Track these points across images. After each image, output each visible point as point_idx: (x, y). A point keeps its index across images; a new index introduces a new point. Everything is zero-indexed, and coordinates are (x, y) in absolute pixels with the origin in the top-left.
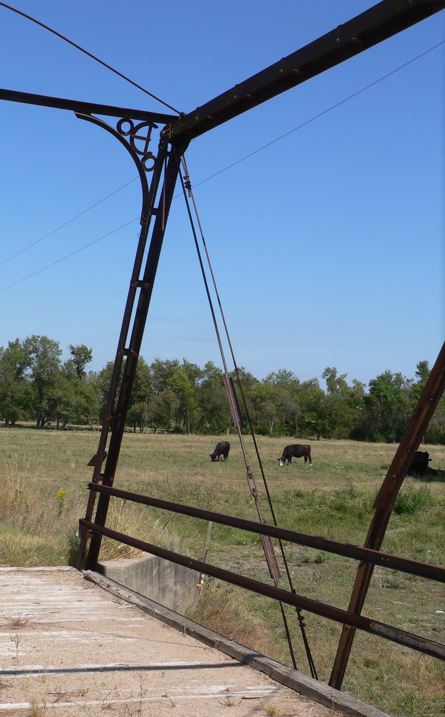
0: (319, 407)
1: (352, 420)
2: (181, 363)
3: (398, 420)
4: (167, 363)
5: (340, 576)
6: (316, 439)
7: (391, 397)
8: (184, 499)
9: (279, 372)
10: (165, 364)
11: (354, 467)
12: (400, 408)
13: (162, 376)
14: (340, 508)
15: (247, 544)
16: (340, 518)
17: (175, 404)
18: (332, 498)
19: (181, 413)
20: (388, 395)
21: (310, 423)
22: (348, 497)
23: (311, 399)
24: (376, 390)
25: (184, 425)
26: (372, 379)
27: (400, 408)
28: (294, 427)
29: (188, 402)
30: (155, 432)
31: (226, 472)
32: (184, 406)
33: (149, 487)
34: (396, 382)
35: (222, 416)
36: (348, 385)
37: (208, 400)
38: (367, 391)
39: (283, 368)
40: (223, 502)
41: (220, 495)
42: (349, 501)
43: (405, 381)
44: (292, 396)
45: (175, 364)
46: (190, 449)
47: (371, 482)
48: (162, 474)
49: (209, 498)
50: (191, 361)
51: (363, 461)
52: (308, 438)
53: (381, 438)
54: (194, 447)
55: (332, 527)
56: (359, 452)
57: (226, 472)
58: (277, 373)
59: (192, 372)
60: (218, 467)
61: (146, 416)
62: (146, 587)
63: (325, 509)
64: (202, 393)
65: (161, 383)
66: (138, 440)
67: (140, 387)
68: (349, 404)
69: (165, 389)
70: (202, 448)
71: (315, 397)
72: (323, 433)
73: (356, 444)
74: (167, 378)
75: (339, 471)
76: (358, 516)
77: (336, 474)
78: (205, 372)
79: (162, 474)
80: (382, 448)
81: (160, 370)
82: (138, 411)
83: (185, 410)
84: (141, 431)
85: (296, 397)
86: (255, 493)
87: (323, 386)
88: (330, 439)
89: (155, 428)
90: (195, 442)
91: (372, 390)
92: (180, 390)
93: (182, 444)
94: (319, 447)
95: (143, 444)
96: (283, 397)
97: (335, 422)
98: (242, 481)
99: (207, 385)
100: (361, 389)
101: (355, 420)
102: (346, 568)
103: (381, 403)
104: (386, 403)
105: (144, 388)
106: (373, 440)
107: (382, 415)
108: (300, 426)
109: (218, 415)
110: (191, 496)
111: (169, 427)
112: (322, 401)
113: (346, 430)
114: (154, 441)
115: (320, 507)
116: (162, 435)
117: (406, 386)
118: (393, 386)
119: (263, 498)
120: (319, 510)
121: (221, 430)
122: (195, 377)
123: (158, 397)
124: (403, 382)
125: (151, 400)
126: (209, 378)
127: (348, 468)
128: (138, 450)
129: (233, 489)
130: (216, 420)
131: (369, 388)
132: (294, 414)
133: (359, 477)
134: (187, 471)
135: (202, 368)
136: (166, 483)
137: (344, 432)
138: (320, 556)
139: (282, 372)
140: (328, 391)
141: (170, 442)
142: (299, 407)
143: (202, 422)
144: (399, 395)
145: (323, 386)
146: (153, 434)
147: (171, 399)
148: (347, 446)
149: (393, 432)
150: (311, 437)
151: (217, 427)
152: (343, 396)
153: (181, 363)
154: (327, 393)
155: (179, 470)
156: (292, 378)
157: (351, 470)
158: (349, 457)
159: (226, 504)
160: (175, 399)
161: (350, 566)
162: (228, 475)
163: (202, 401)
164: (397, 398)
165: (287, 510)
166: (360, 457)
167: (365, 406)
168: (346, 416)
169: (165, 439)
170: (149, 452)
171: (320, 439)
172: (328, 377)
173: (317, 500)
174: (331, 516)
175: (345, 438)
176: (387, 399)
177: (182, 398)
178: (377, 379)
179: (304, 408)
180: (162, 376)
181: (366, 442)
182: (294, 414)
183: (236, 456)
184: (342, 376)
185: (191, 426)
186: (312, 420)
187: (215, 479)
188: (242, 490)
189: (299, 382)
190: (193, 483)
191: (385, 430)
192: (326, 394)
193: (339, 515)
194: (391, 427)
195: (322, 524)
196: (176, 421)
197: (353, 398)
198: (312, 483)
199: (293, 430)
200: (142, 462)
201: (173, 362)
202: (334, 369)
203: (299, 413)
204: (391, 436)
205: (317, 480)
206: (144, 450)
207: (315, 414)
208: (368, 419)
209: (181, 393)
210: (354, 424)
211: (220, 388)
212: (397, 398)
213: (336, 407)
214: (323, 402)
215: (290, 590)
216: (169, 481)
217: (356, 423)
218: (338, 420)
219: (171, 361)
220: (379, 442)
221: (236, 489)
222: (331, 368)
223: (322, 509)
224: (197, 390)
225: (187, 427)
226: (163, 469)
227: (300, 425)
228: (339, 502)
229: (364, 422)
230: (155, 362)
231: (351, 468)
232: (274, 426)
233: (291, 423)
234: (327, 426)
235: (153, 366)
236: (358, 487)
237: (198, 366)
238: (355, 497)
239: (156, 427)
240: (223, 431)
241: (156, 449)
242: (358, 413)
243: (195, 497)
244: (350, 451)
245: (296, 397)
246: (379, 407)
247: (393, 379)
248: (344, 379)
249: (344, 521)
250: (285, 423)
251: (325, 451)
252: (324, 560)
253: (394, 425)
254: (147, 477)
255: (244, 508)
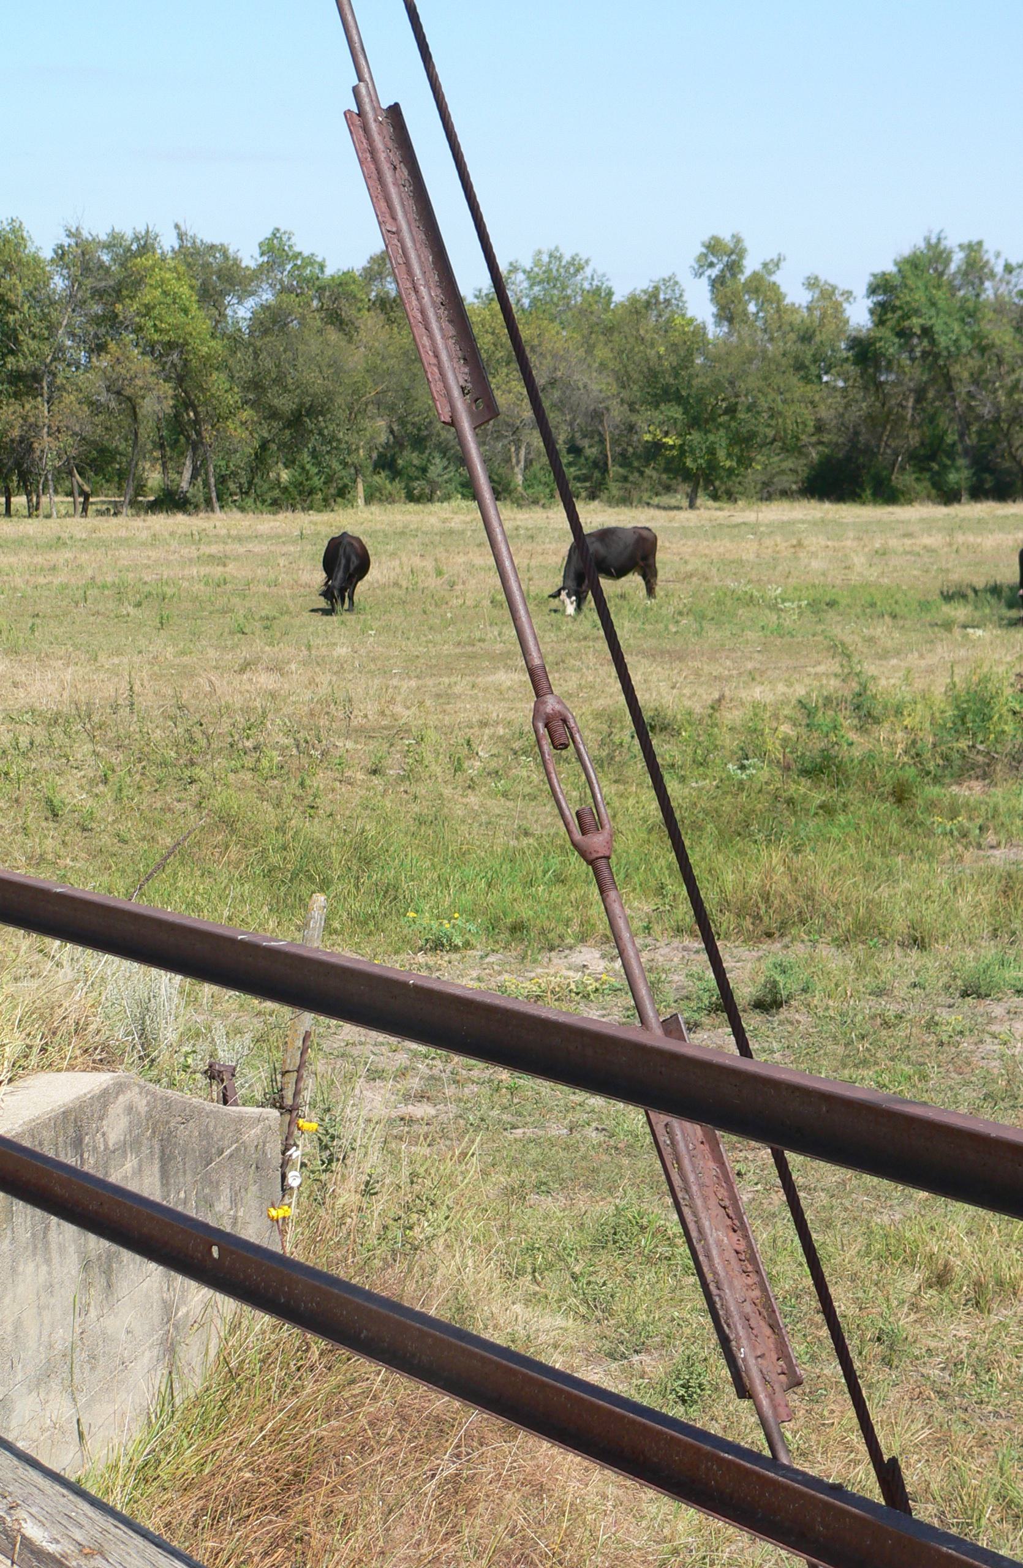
0: (690, 386)
1: (811, 429)
2: (168, 242)
3: (979, 417)
4: (113, 243)
5: (864, 1063)
6: (685, 503)
7: (949, 332)
8: (203, 774)
9: (537, 262)
10: (108, 246)
11: (844, 602)
12: (982, 371)
13: (98, 294)
14: (821, 768)
15: (467, 945)
16: (827, 809)
17: (157, 401)
18: (785, 729)
19: (182, 434)
20: (936, 329)
21: (657, 447)
22: (847, 722)
23: (660, 357)
24: (894, 309)
25: (194, 477)
26: (878, 270)
27: (982, 371)
28: (600, 465)
29: (203, 390)
30: (85, 510)
31: (363, 652)
32: (189, 404)
33: (58, 733)
34: (966, 274)
35: (334, 438)
36: (788, 300)
37: (278, 381)
38: (859, 315)
39: (547, 246)
40: (360, 776)
41: (350, 745)
42: (852, 736)
43: (999, 269)
44: (590, 350)
45: (146, 245)
46: (220, 569)
47: (922, 656)
48: (115, 672)
49: (305, 761)
50: (207, 234)
51: (873, 574)
52: (656, 500)
53: (918, 487)
54: (237, 558)
55: (797, 851)
56: (849, 543)
57: (363, 652)
58: (527, 264)
59: (213, 276)
60: (338, 637)
61: (49, 450)
62: (14, 1270)
63: (761, 772)
64: (256, 355)
65: (98, 321)
66: (20, 543)
67: (16, 341)
68: (799, 366)
69: (112, 346)
70: (266, 561)
71: (673, 347)
72: (706, 480)
73: (830, 516)
74: (119, 299)
75: (789, 621)
76: (893, 793)
77: (780, 631)
78: (264, 270)
79: (115, 672)
80: (928, 525)
81: (86, 270)
82: (16, 433)
83: (196, 422)
84: (33, 510)
85: (602, 352)
86: (597, 842)
87: (699, 306)
88: (736, 501)
89: (86, 496)
90: (239, 539)
91: (881, 312)
92: (170, 346)
93: (191, 551)
94: (689, 533)
95: (39, 559)
96: (554, 356)
97: (753, 435)
98: (430, 682)
99: (271, 321)
100: (838, 309)
101: (820, 428)
102: (886, 1024)
103: (913, 359)
104: (931, 356)
105: (34, 345)
106: (887, 494)
107: (918, 401)
108: (624, 460)
109: (320, 434)
110: (230, 757)
111: (140, 489)
112: (699, 361)
113: (789, 464)
114: (85, 544)
115: (743, 767)
116: (114, 521)
117: (1003, 289)
118: (953, 289)
119: (516, 745)
120: (741, 782)
121: (333, 491)
122: (223, 294)
123: (86, 375)
124: (992, 275)
125: (62, 388)
126: (275, 295)
127: (823, 605)
128: (19, 582)
129: (395, 717)
130: (314, 454)
131: (869, 303)
132: (597, 416)
133: (871, 640)
134: (212, 653)
135: (249, 257)
136: (124, 712)
137: (783, 472)
138: (775, 984)
139: (545, 258)
140: (718, 324)
141: (143, 544)
142: (614, 389)
143: (260, 459)
144: (977, 321)
145: (699, 306)
146: (78, 520)
147: (139, 382)
148: (803, 522)
149: (961, 462)
150: (665, 500)
151: (317, 482)
152: (771, 339)
153: (168, 242)
154: (714, 331)
155: (183, 653)
156: (584, 281)
157: (831, 615)
158: (815, 564)
159: (376, 780)
160: (152, 380)
161: (899, 1017)
162: (373, 660)
163: (255, 385)
164: (973, 336)
165: (614, 788)
166: (859, 561)
167: (852, 369)
168: (789, 411)
169: (123, 533)
170: (65, 587)
171: (699, 502)
172: (714, 272)
173: (729, 742)
174: (790, 801)
175: (785, 494)
176: (933, 342)
177: (182, 378)
178: (894, 269)
179: (635, 392)
180: (98, 294)
181: (864, 503)
182: (597, 416)
183: (396, 584)
184: (765, 265)
185: (222, 480)
186: (666, 434)
187: (324, 679)
188: (432, 720)
189: (610, 293)
190: (238, 702)
191: (932, 457)
192: (710, 336)
193: (818, 797)
194: (954, 445)
195: (760, 837)
196: (164, 465)
197: (807, 346)
198: (697, 673)
199: (597, 474)
200: (32, 629)
201: (137, 238)
202: (738, 240)
203: (617, 413)
204: (952, 477)
205: (713, 659)
206: (42, 580)
207: (676, 412)
208: (870, 417)
209: (175, 357)
210: (820, 443)
211: (320, 332)
212: (973, 336)
213: (753, 382)
214: (703, 366)
215: (865, 1482)
216: (142, 703)
217: (826, 438)
218: (762, 429)
219: (129, 235)
220: (910, 502)
221: (406, 715)
222: (726, 236)
223: (751, 777)
224: (235, 341)
225: (206, 484)
226: (118, 652)
227: (623, 455)
228: (816, 744)
229: (856, 433)
230: (66, 241)
231: (831, 604)
232: (529, 463)
233: (592, 452)
234: (721, 454)
235: (61, 254)
236: (887, 680)
237: (231, 251)
238: (877, 721)
239: (87, 488)
240: (343, 493)
241: (90, 573)
242: (827, 403)
243: (249, 761)
244: (815, 541)
245: (602, 352)
246: (904, 372)
247: (953, 267)
248: (773, 278)
249: (842, 818)
250: (569, 451)
251: (722, 546)
252: (790, 996)
253: (962, 435)
254: (52, 688)
255: (447, 791)
